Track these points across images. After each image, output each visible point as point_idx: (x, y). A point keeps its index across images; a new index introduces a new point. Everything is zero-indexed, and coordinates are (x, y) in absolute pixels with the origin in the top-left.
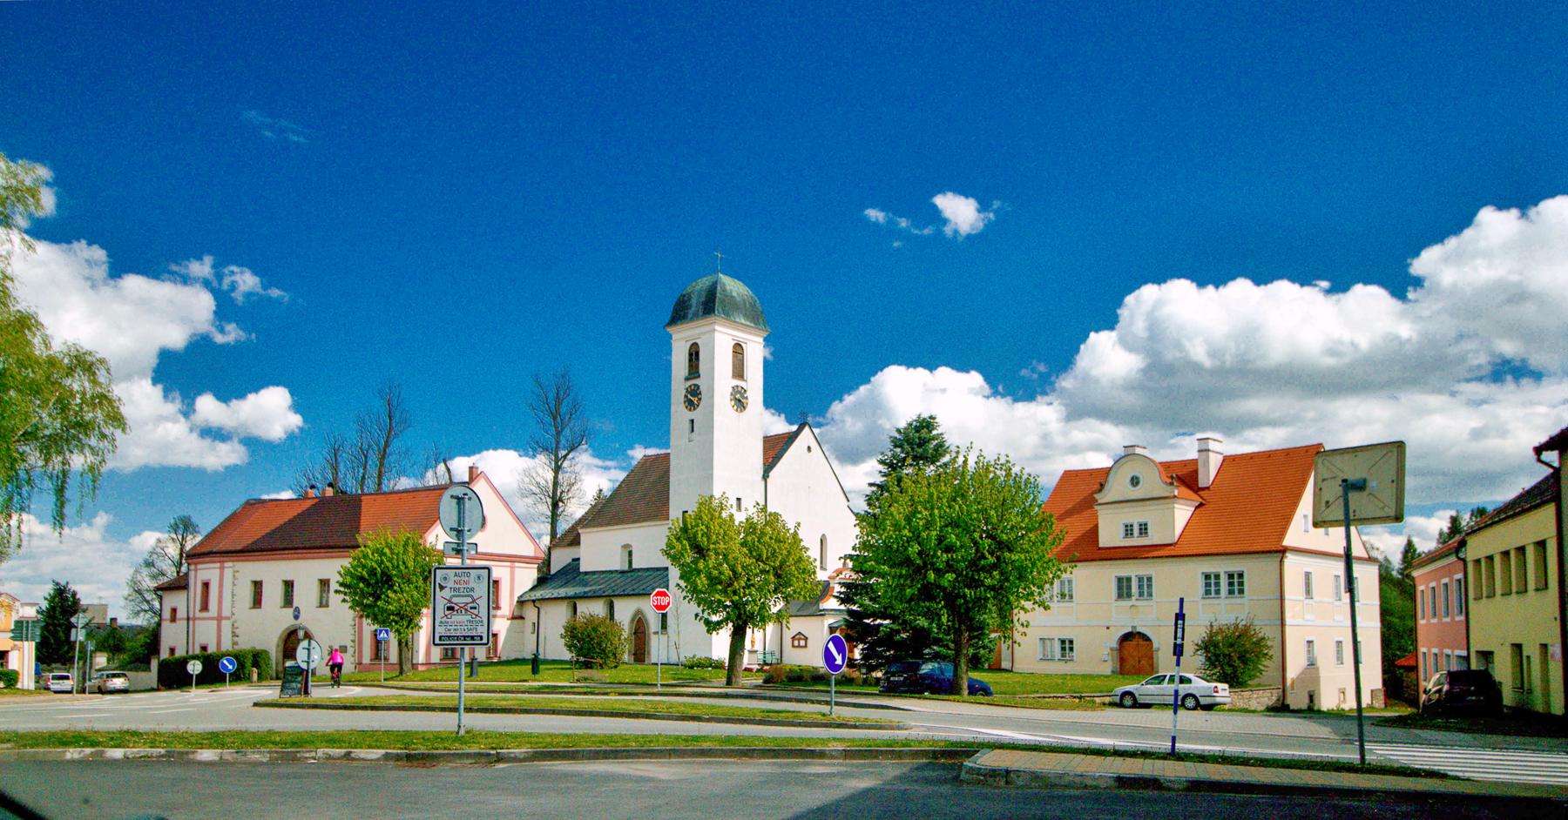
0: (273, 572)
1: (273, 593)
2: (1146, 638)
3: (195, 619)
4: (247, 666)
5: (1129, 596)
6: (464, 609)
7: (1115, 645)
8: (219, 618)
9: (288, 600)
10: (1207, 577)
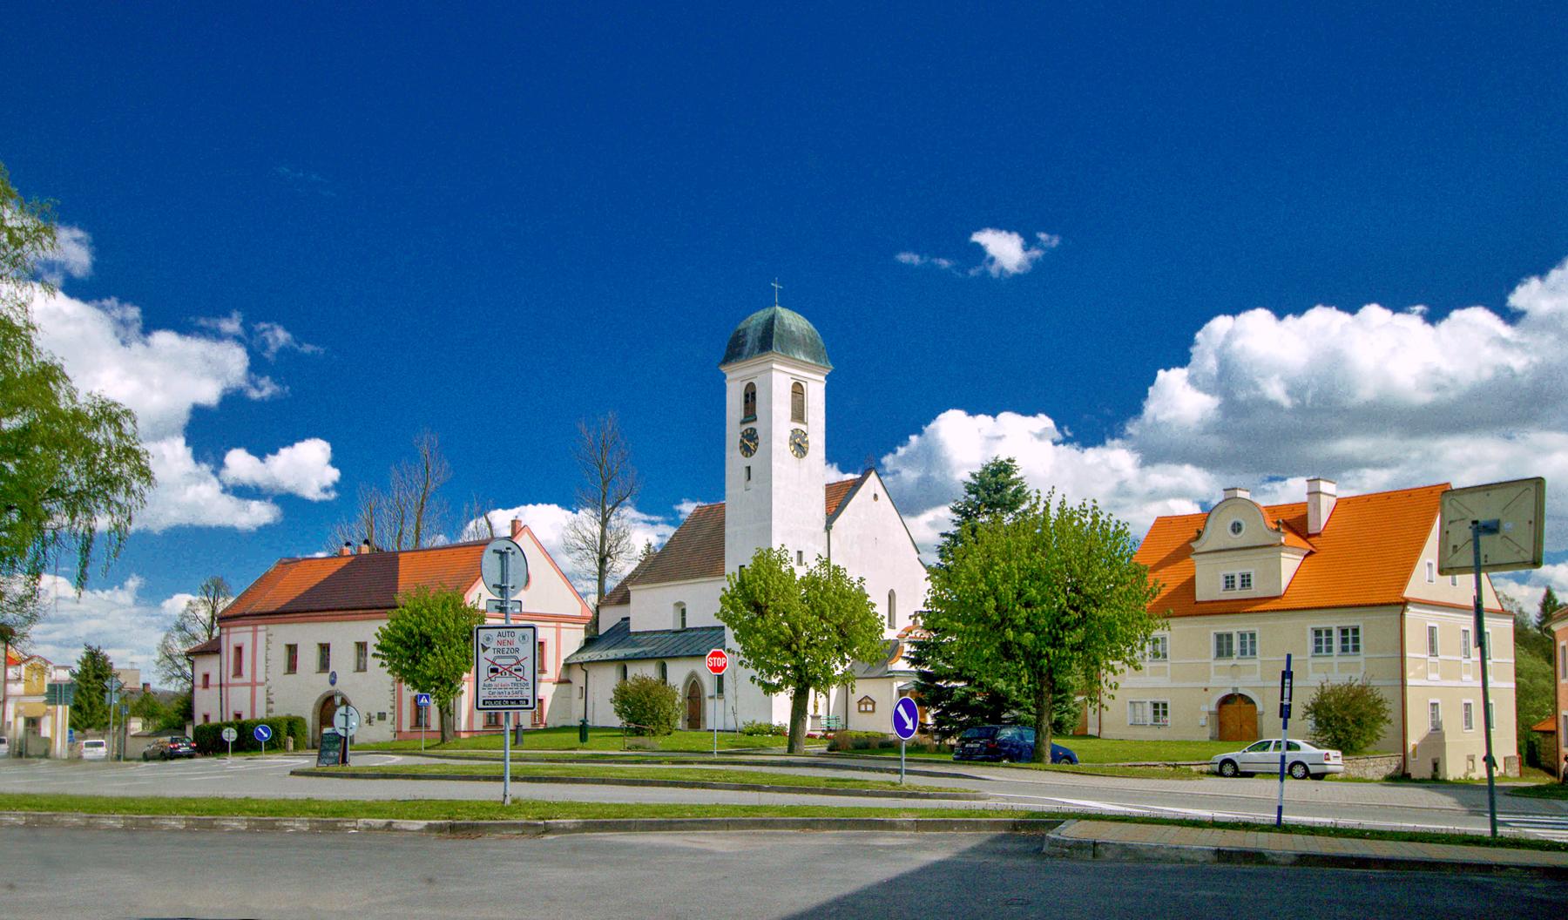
0: (308, 635)
1: (308, 658)
2: (1251, 702)
3: (228, 685)
4: (273, 735)
5: (1230, 654)
6: (508, 671)
7: (1213, 708)
8: (253, 684)
9: (324, 665)
10: (1318, 632)
